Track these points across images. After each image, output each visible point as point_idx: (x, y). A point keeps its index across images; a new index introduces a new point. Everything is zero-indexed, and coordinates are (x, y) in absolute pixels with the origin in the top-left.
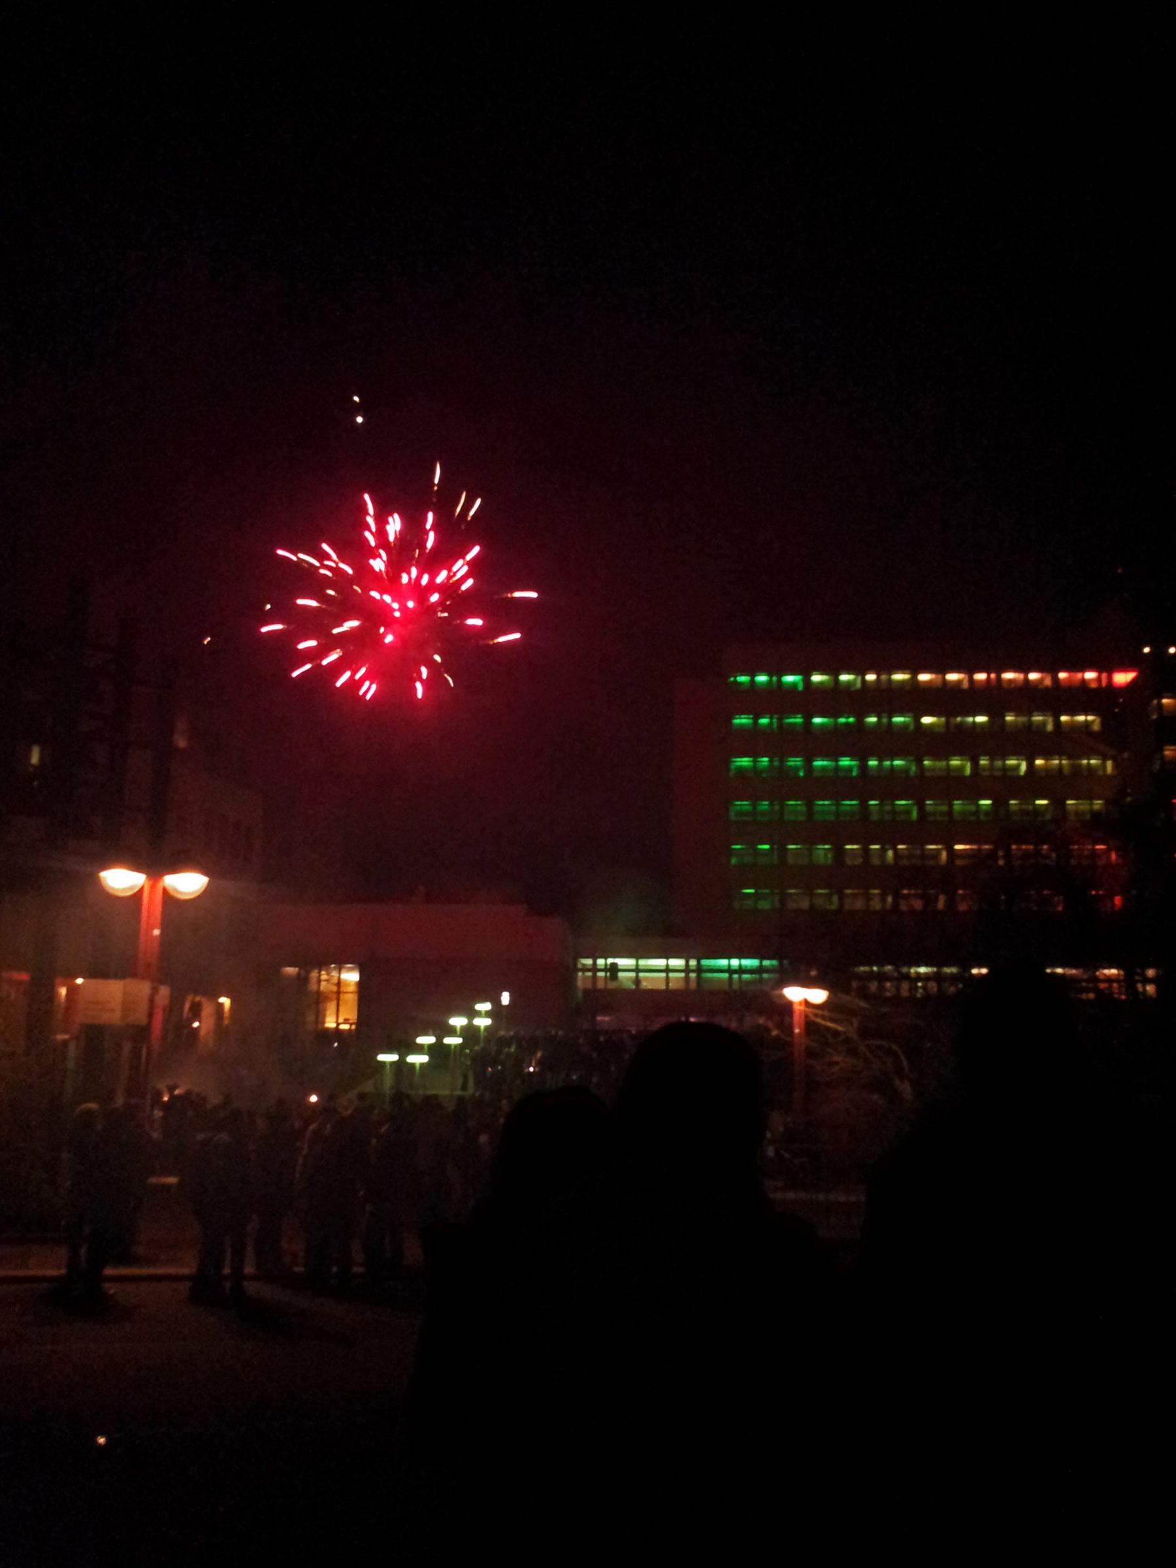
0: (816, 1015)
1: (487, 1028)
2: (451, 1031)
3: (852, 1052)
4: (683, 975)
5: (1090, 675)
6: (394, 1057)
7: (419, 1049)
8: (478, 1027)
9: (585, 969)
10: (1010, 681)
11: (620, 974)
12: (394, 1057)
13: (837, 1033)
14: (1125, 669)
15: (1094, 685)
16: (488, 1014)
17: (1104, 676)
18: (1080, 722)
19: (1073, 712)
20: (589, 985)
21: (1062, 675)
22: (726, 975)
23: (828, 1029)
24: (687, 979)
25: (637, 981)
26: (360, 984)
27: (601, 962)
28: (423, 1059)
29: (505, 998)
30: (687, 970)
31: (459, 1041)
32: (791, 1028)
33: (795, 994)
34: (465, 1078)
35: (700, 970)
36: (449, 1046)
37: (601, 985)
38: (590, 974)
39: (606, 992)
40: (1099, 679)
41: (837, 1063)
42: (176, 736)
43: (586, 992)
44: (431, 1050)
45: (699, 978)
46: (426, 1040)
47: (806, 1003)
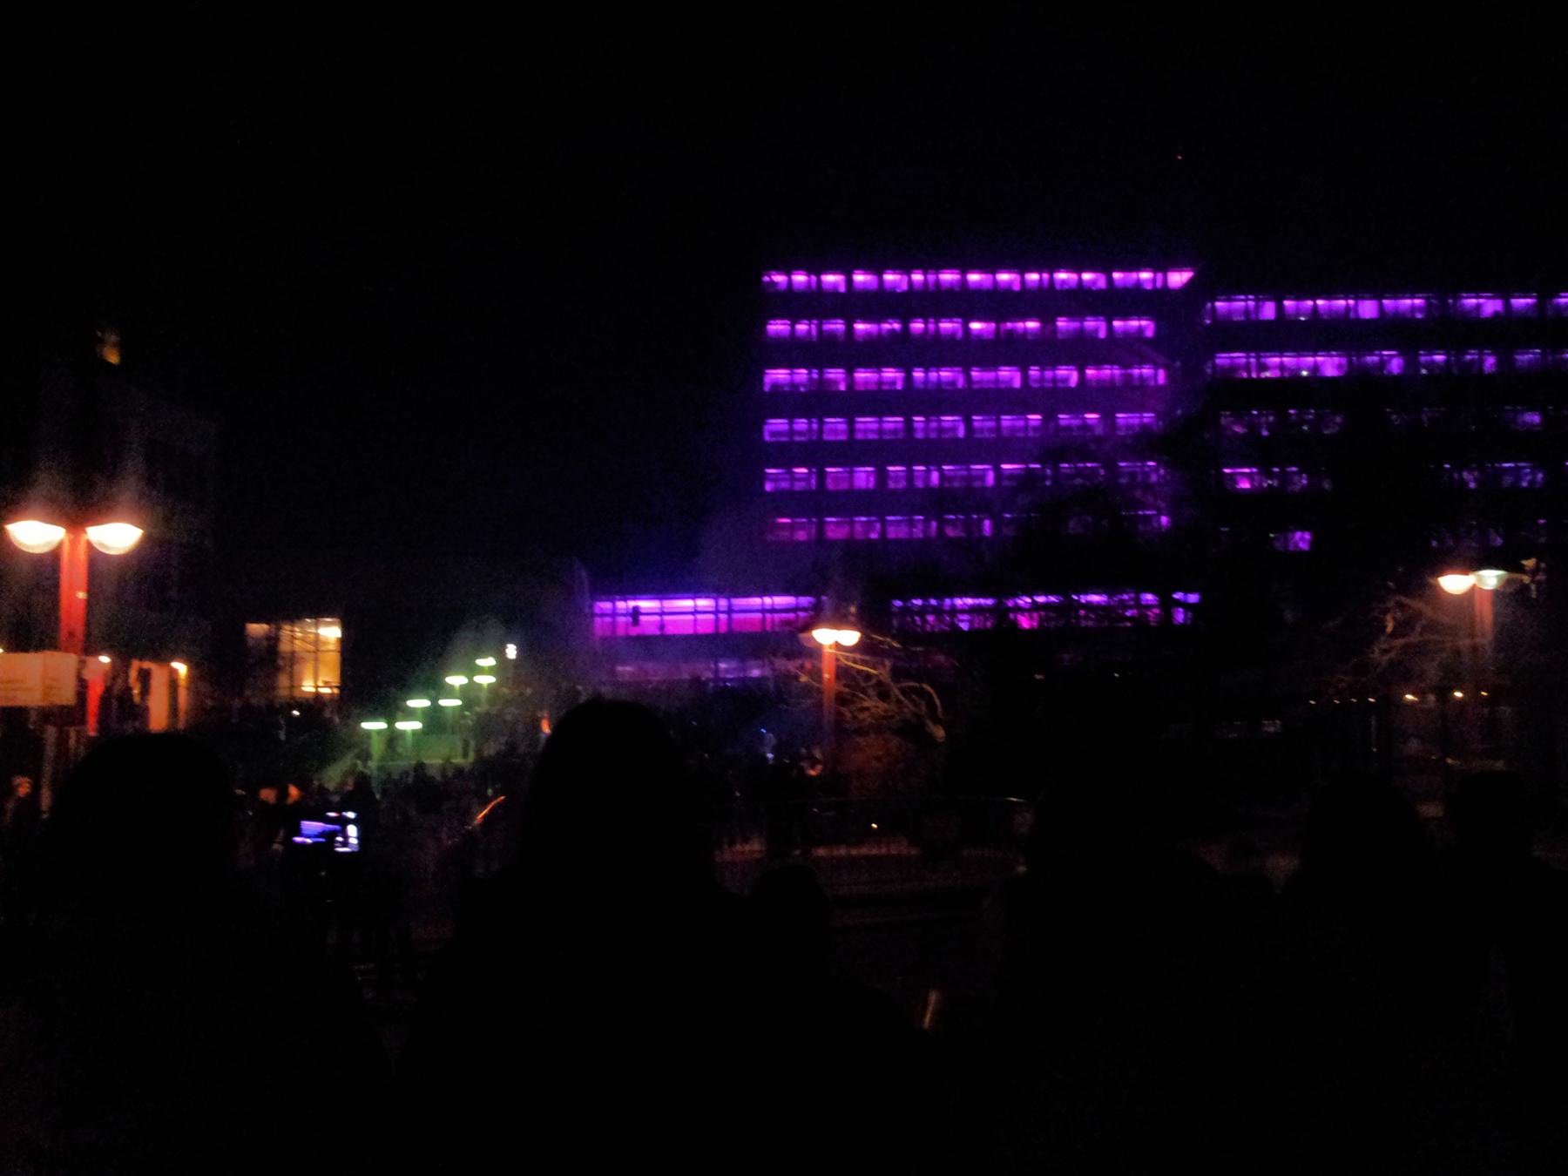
0: (847, 658)
2: (450, 692)
3: (884, 695)
9: (603, 615)
11: (643, 618)
15: (1149, 287)
20: (608, 633)
23: (859, 672)
25: (662, 626)
26: (343, 642)
28: (416, 725)
30: (716, 612)
32: (820, 676)
35: (730, 611)
38: (608, 619)
40: (1154, 280)
41: (867, 709)
43: (604, 639)
45: (730, 619)
46: (419, 703)
47: (838, 645)
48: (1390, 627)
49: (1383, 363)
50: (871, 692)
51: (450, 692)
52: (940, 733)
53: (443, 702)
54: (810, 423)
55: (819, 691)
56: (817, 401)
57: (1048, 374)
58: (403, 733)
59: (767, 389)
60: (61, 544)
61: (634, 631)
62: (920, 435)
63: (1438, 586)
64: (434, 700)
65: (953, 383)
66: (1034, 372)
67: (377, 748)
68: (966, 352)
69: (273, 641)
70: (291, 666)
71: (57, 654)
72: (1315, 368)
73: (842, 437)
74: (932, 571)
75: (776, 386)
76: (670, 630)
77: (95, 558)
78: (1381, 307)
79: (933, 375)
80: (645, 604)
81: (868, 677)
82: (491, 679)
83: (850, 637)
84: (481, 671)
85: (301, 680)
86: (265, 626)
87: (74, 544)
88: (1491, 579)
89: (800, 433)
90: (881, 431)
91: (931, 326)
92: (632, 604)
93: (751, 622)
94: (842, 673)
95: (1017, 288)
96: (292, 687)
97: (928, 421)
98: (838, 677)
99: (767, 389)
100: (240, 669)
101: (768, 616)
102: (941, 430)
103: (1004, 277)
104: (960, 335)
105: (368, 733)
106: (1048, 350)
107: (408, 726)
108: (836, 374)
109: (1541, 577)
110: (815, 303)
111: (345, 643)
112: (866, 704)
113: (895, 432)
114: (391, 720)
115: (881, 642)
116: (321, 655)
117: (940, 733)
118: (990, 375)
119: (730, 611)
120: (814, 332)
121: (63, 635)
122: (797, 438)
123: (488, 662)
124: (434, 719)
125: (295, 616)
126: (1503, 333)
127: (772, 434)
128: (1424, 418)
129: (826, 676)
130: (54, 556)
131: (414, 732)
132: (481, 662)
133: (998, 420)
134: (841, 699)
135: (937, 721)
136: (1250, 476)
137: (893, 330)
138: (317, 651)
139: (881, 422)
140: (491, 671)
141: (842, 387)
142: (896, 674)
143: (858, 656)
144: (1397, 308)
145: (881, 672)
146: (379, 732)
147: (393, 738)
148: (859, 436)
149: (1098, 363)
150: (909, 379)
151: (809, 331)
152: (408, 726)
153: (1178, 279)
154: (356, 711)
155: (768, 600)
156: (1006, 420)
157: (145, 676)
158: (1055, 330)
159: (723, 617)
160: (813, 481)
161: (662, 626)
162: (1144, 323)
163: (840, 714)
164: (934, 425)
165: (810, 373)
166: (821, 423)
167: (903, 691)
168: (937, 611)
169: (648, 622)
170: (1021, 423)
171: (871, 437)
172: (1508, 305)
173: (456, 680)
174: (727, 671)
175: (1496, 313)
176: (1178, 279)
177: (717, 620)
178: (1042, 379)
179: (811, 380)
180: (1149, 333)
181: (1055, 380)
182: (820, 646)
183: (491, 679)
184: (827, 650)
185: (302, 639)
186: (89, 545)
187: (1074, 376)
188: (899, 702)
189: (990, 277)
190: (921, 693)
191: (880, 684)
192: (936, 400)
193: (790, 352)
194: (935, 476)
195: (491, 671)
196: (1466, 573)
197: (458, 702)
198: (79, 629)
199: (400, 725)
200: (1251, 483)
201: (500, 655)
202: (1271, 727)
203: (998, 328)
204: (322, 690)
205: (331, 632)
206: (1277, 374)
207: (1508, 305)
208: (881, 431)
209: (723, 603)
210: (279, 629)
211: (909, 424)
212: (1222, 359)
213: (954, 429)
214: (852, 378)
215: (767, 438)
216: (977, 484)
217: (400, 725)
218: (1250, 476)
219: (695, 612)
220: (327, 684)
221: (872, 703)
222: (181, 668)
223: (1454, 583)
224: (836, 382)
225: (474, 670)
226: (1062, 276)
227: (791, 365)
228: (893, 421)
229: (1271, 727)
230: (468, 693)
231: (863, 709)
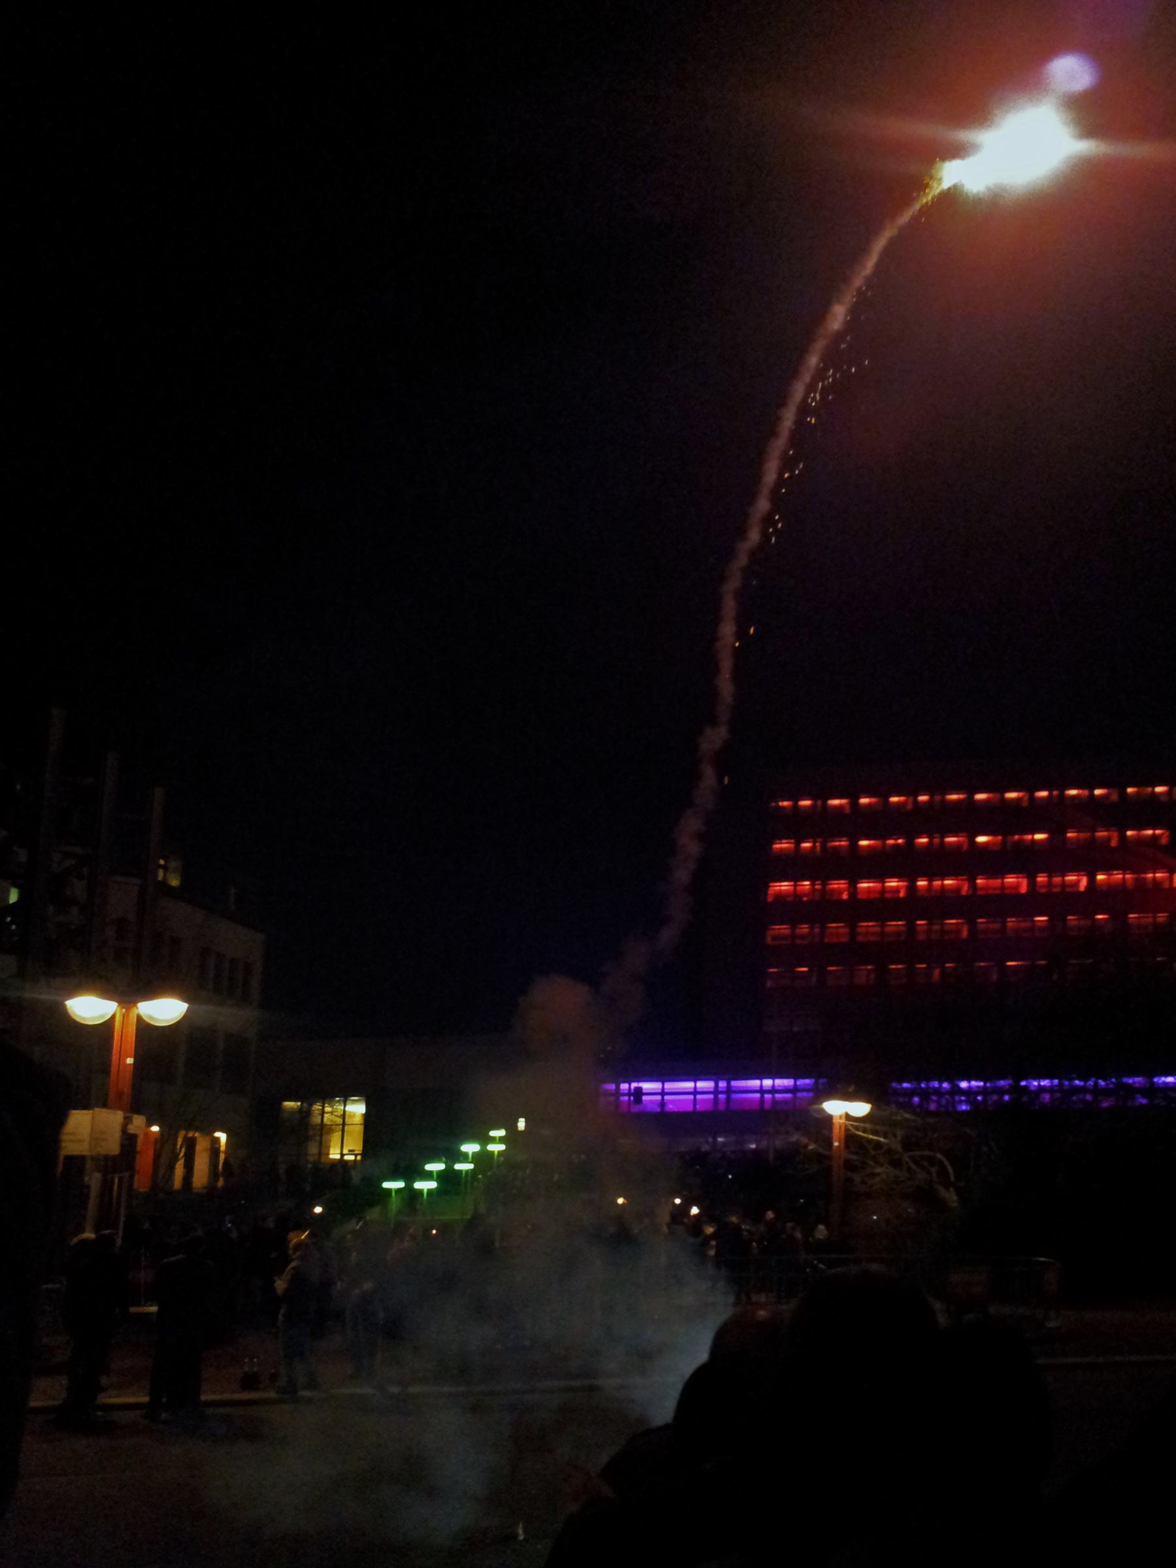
0: (857, 1128)
2: (464, 1158)
3: (896, 1163)
4: (711, 1096)
7: (428, 1176)
9: (607, 1094)
10: (1074, 797)
12: (400, 1184)
17: (819, 802)
23: (870, 1141)
25: (663, 1103)
26: (366, 1117)
28: (433, 1185)
30: (716, 1091)
32: (830, 1144)
35: (729, 1090)
36: (461, 1171)
41: (879, 1174)
44: (442, 1177)
45: (728, 1100)
47: (848, 1117)
50: (881, 1159)
51: (464, 1158)
52: (951, 1197)
53: (458, 1167)
54: (812, 928)
55: (829, 1158)
56: (821, 909)
57: (1057, 880)
58: (420, 1192)
59: (770, 899)
60: (113, 1017)
61: (635, 1109)
62: (922, 937)
65: (957, 890)
66: (1041, 879)
67: (395, 1204)
68: (970, 862)
69: (305, 1114)
70: (321, 1136)
71: (104, 1110)
73: (845, 939)
75: (780, 896)
77: (145, 1030)
79: (937, 883)
80: (646, 1086)
81: (878, 1145)
82: (502, 1147)
83: (861, 1109)
84: (493, 1140)
85: (328, 1148)
87: (125, 1017)
89: (802, 937)
90: (882, 934)
91: (936, 840)
92: (634, 1085)
93: (752, 1100)
94: (850, 1139)
95: (1025, 804)
96: (320, 1154)
97: (930, 924)
98: (847, 1146)
99: (770, 899)
100: (275, 1143)
101: (767, 1096)
102: (943, 932)
103: (892, 883)
104: (965, 846)
105: (389, 1191)
106: (1057, 857)
107: (424, 1186)
108: (838, 885)
110: (821, 824)
111: (369, 1120)
113: (899, 934)
114: (410, 1180)
117: (951, 1197)
118: (997, 882)
119: (729, 1090)
120: (818, 849)
121: (112, 1095)
122: (798, 942)
124: (448, 1179)
125: (327, 1096)
127: (775, 938)
129: (836, 1144)
130: (107, 1027)
131: (430, 1192)
132: (493, 1133)
133: (1004, 923)
134: (849, 1165)
135: (947, 1185)
137: (897, 845)
138: (344, 1124)
139: (883, 926)
140: (501, 1140)
141: (845, 896)
142: (907, 1144)
143: (868, 1126)
146: (398, 1191)
147: (411, 1196)
148: (860, 939)
149: (1107, 868)
150: (912, 888)
151: (813, 848)
152: (424, 1186)
155: (768, 1083)
156: (1011, 922)
157: (191, 1144)
158: (1065, 839)
159: (722, 1097)
160: (814, 979)
161: (663, 1103)
162: (1158, 832)
163: (850, 1180)
164: (936, 927)
165: (813, 885)
166: (823, 927)
167: (911, 1158)
169: (652, 1102)
170: (1028, 924)
171: (873, 939)
173: (470, 1148)
174: (724, 1144)
177: (716, 1100)
178: (1050, 884)
179: (813, 890)
180: (1164, 841)
181: (1064, 885)
182: (830, 1118)
183: (502, 1147)
184: (837, 1121)
185: (332, 1113)
186: (139, 1018)
187: (1084, 881)
188: (909, 1169)
189: (998, 795)
190: (932, 1161)
191: (889, 1152)
192: (943, 904)
193: (793, 867)
194: (936, 974)
195: (501, 1140)
197: (471, 1166)
198: (127, 1090)
199: (418, 1185)
201: (511, 1127)
203: (1004, 842)
204: (346, 1158)
205: (357, 1109)
208: (882, 934)
209: (722, 1084)
210: (311, 1105)
211: (911, 927)
213: (958, 931)
214: (856, 888)
215: (769, 940)
217: (418, 1185)
219: (695, 1092)
220: (351, 1152)
221: (883, 1171)
222: (222, 1137)
224: (840, 892)
225: (485, 1140)
227: (796, 878)
228: (896, 925)
230: (482, 1159)
231: (873, 1175)
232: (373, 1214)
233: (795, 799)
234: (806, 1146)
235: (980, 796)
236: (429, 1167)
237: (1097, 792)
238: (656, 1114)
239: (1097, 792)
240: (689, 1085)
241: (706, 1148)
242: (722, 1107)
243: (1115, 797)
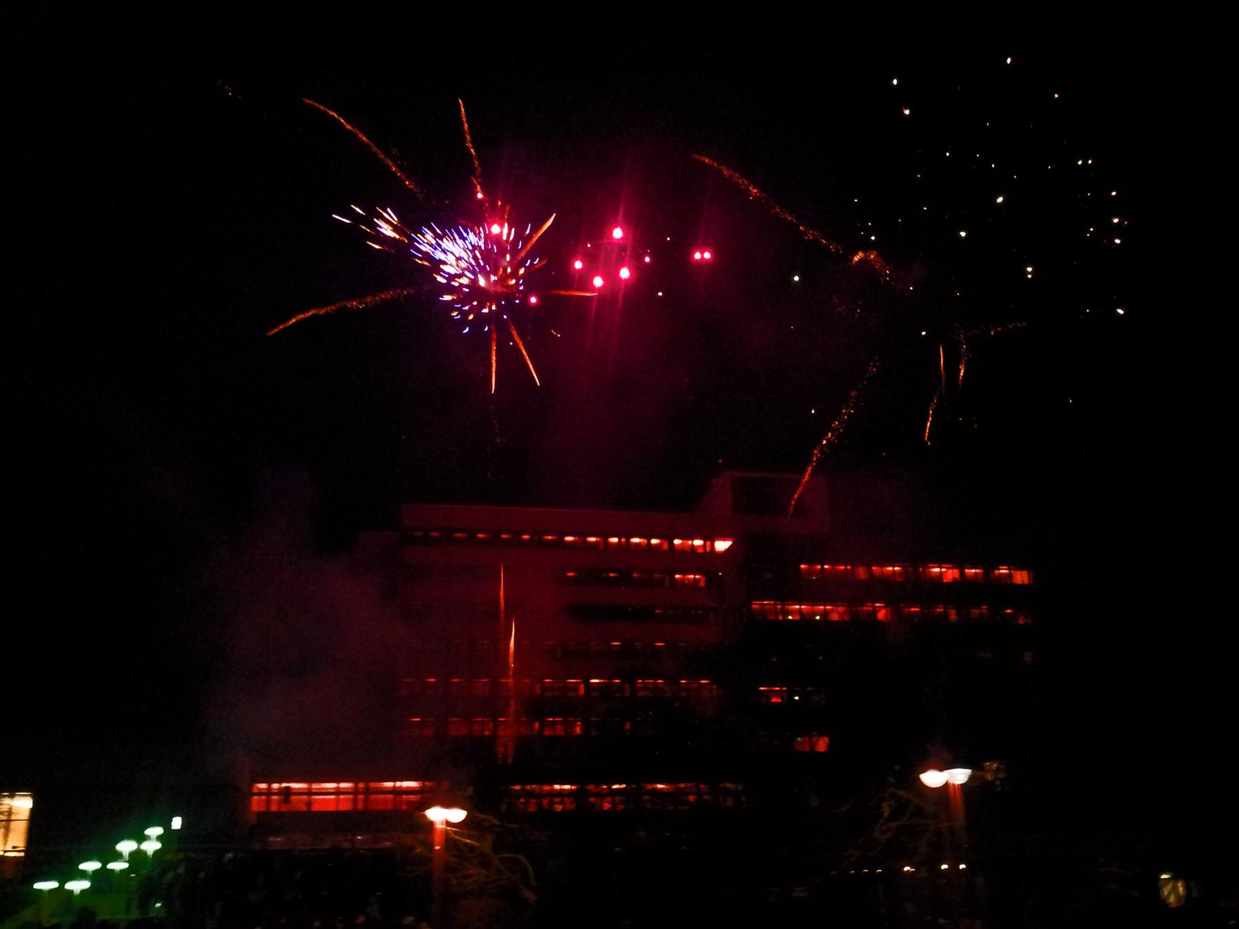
0: (455, 832)
1: (156, 852)
2: (118, 856)
3: (486, 864)
4: (350, 796)
5: (698, 542)
6: (53, 885)
7: (83, 875)
8: (72, 892)
9: (260, 793)
10: (637, 544)
11: (293, 797)
12: (53, 885)
13: (472, 849)
14: (724, 538)
15: (701, 551)
16: (159, 838)
17: (708, 543)
18: (689, 580)
19: (685, 573)
20: (263, 809)
21: (677, 542)
22: (390, 796)
23: (467, 844)
24: (355, 801)
25: (309, 803)
26: (33, 812)
27: (275, 786)
28: (85, 884)
29: (177, 823)
30: (355, 792)
31: (125, 865)
32: (432, 845)
33: (439, 815)
34: (130, 900)
35: (368, 792)
36: (40, 891)
37: (274, 808)
38: (264, 797)
39: (279, 815)
40: (704, 545)
41: (471, 876)
42: (152, 914)
43: (259, 814)
44: (95, 876)
45: (366, 800)
46: (91, 866)
47: (448, 823)
48: (886, 812)
49: (875, 611)
51: (118, 856)
52: (531, 896)
63: (425, 816)
64: (104, 864)
72: (825, 614)
74: (539, 761)
76: (315, 808)
78: (871, 572)
82: (158, 846)
83: (457, 815)
86: (968, 772)
88: (959, 776)
109: (1001, 775)
112: (470, 872)
115: (483, 820)
116: (13, 824)
117: (531, 896)
123: (155, 831)
126: (960, 592)
128: (387, 231)
136: (780, 694)
144: (882, 573)
145: (486, 845)
152: (77, 886)
153: (722, 546)
154: (169, 857)
167: (501, 860)
168: (531, 794)
172: (962, 574)
173: (126, 847)
175: (954, 579)
176: (722, 546)
182: (432, 823)
196: (941, 770)
199: (70, 886)
200: (782, 698)
201: (167, 825)
202: (800, 893)
206: (797, 617)
207: (962, 574)
209: (361, 785)
212: (756, 605)
216: (571, 694)
217: (70, 886)
218: (780, 694)
219: (338, 792)
223: (932, 779)
225: (141, 838)
226: (636, 540)
229: (800, 893)
230: (137, 856)
232: (27, 915)
233: (710, 538)
234: (412, 849)
235: (636, 540)
236: (83, 866)
237: (654, 541)
238: (304, 812)
239: (654, 541)
240: (332, 785)
241: (347, 845)
242: (360, 806)
243: (666, 546)
